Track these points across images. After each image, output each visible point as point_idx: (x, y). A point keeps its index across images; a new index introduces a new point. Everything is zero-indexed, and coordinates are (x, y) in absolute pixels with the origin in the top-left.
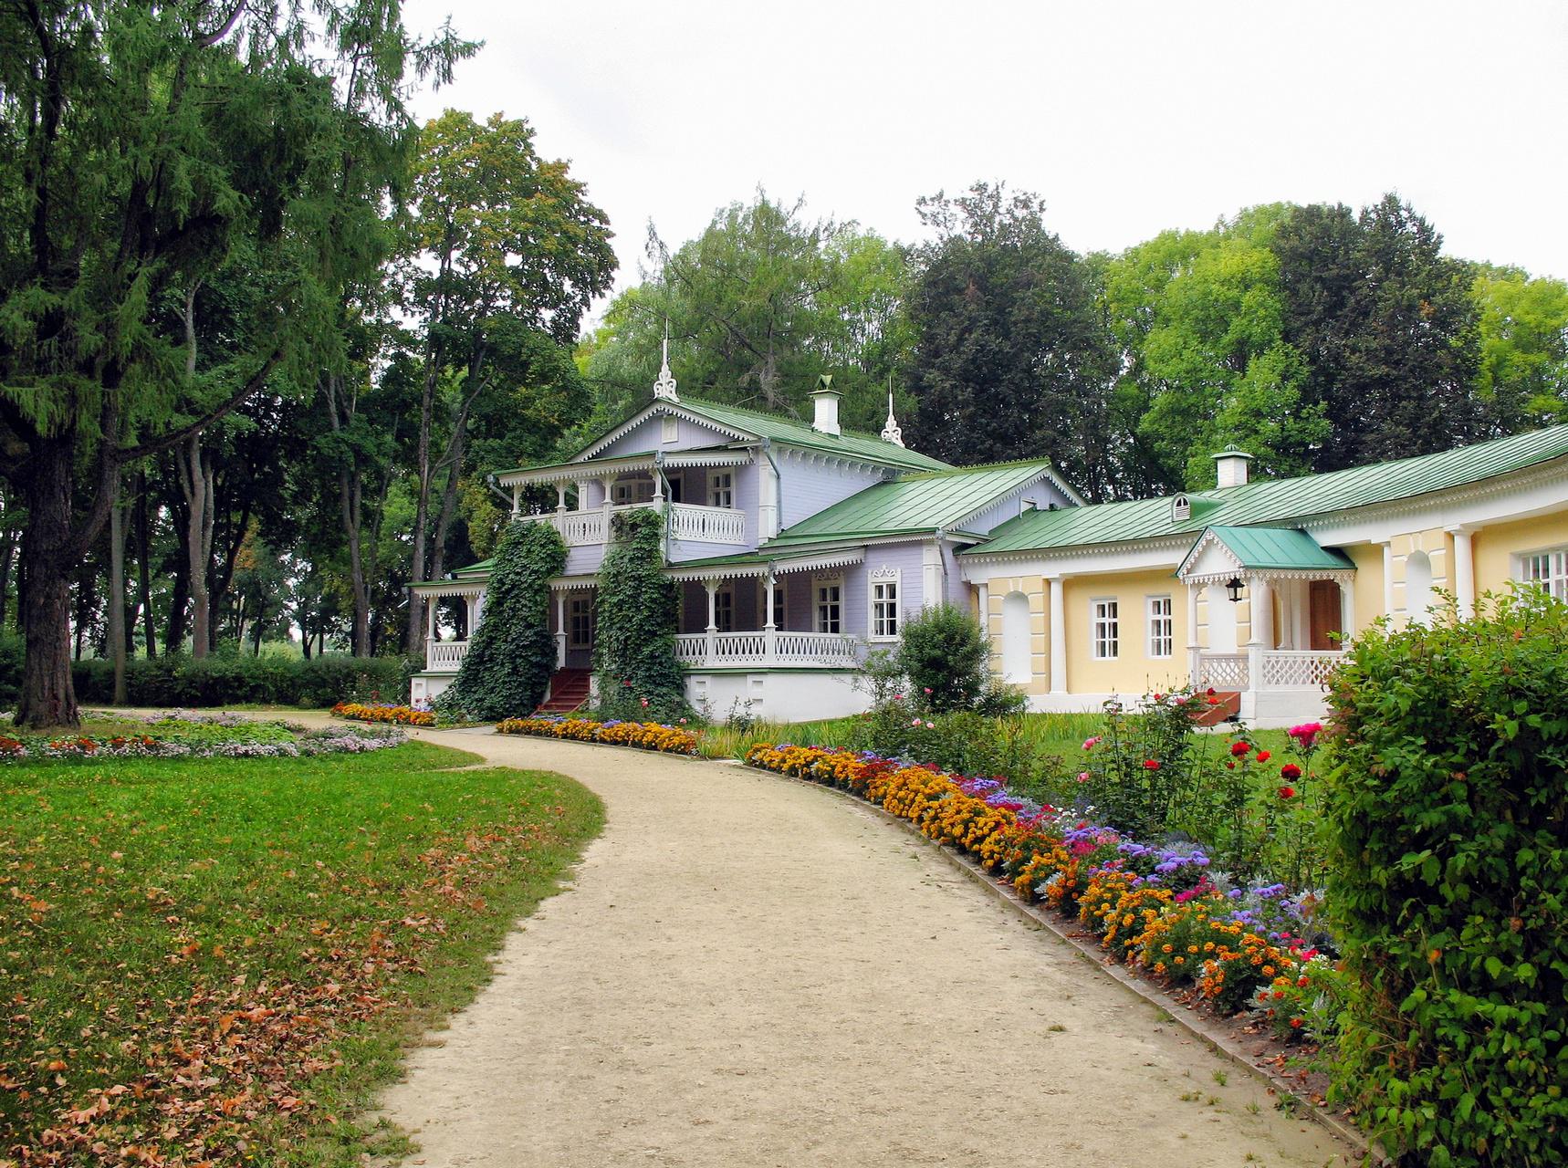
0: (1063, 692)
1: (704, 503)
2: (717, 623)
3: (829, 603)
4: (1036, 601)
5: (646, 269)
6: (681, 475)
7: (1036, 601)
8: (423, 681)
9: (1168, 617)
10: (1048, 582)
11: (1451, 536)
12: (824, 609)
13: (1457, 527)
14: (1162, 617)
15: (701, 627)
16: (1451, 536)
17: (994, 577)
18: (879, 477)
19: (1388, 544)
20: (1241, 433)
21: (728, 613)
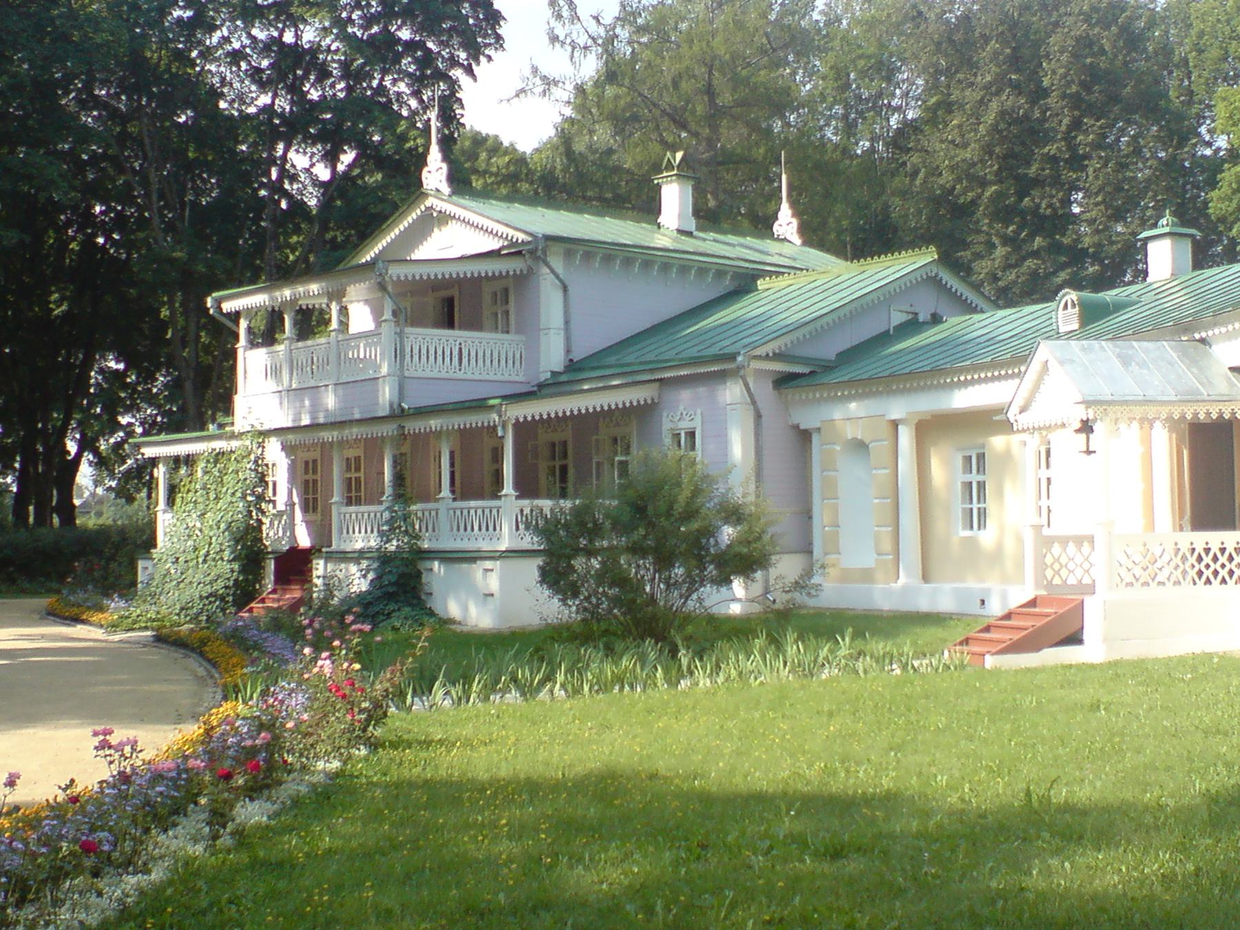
0: (916, 581)
5: (556, 32)
6: (455, 292)
7: (880, 448)
9: (981, 478)
10: (895, 424)
14: (974, 478)
16: (895, 424)
18: (727, 284)
19: (819, 430)
21: (315, 500)
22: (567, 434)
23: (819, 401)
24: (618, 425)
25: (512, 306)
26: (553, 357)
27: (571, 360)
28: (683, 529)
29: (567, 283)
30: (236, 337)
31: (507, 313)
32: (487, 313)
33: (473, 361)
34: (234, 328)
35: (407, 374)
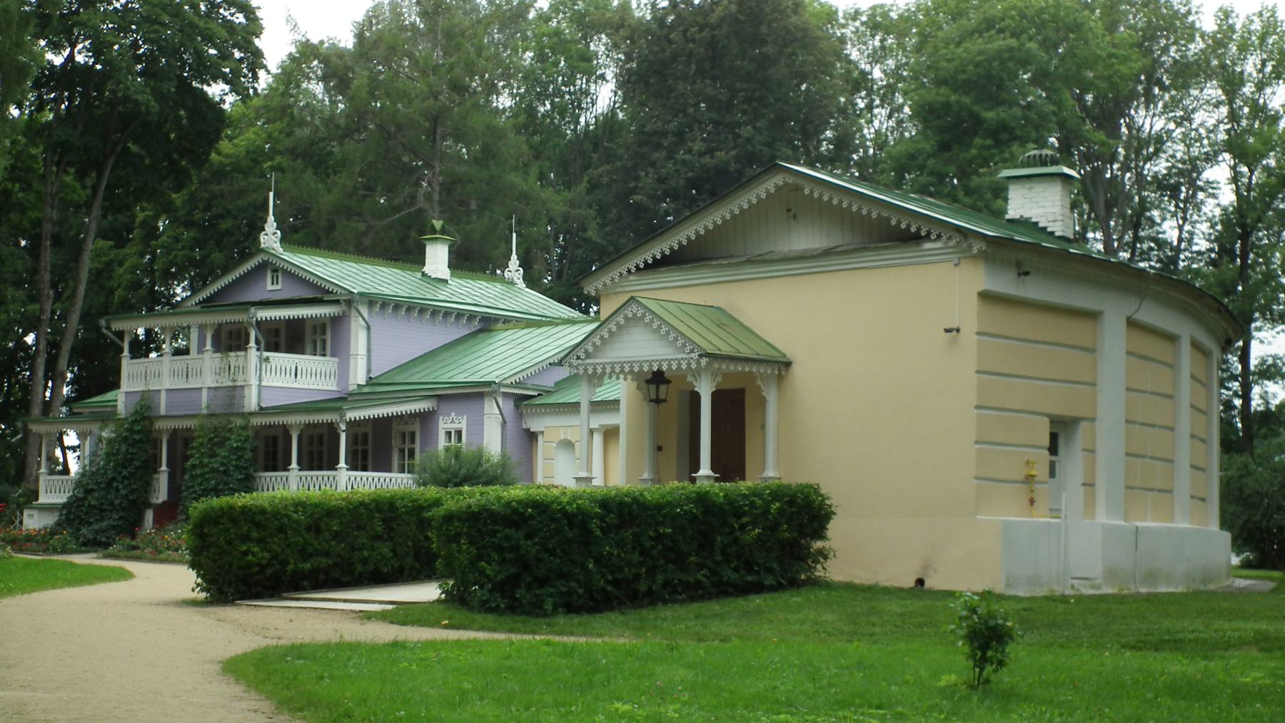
1: (302, 353)
2: (299, 463)
3: (407, 446)
4: (580, 448)
7: (580, 448)
8: (35, 513)
11: (591, 432)
12: (402, 451)
13: (597, 426)
15: (285, 467)
16: (591, 432)
17: (550, 428)
18: (476, 325)
19: (542, 432)
20: (1215, 185)
22: (369, 429)
23: (543, 414)
24: (406, 423)
25: (328, 337)
26: (359, 376)
27: (371, 378)
28: (1277, 459)
29: (370, 323)
30: (122, 351)
31: (324, 342)
32: (308, 340)
33: (304, 375)
34: (119, 342)
35: (264, 384)
